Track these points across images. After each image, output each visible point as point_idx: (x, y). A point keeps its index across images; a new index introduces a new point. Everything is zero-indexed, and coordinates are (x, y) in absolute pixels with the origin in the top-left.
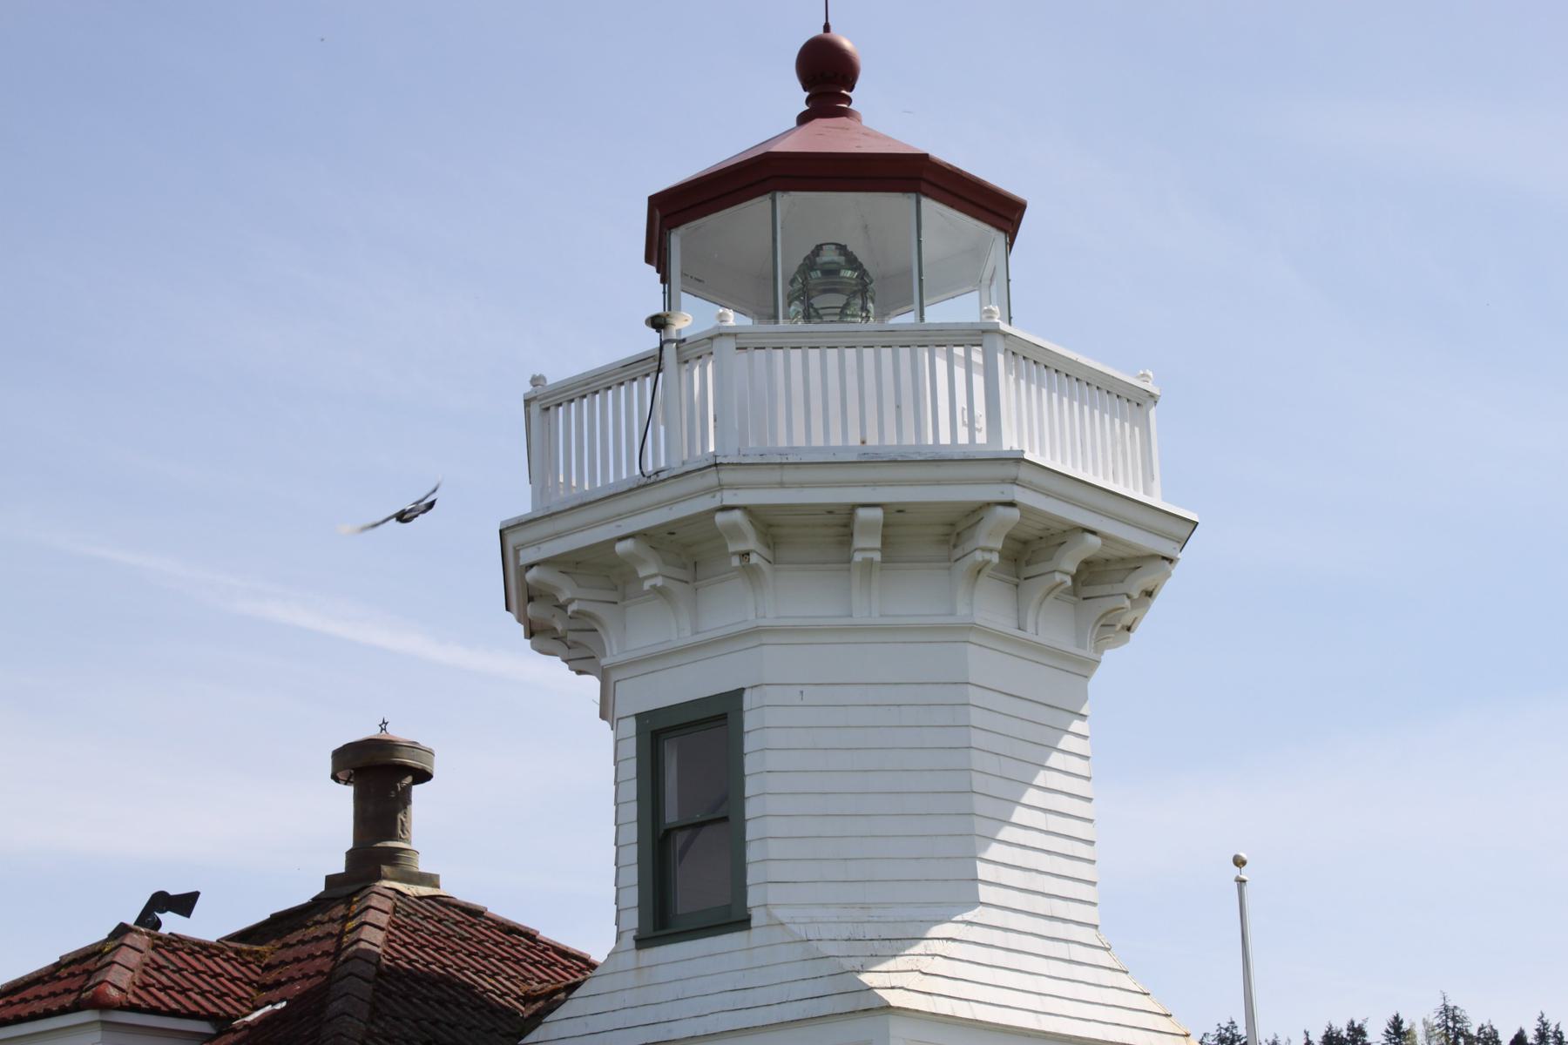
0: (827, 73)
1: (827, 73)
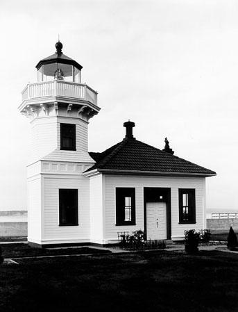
0: (59, 46)
1: (59, 46)
